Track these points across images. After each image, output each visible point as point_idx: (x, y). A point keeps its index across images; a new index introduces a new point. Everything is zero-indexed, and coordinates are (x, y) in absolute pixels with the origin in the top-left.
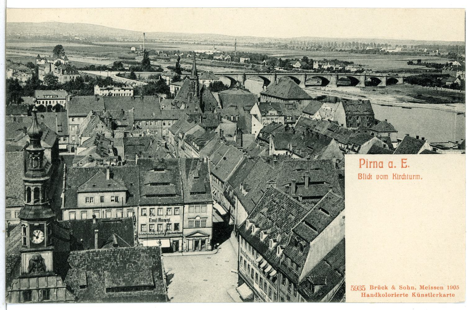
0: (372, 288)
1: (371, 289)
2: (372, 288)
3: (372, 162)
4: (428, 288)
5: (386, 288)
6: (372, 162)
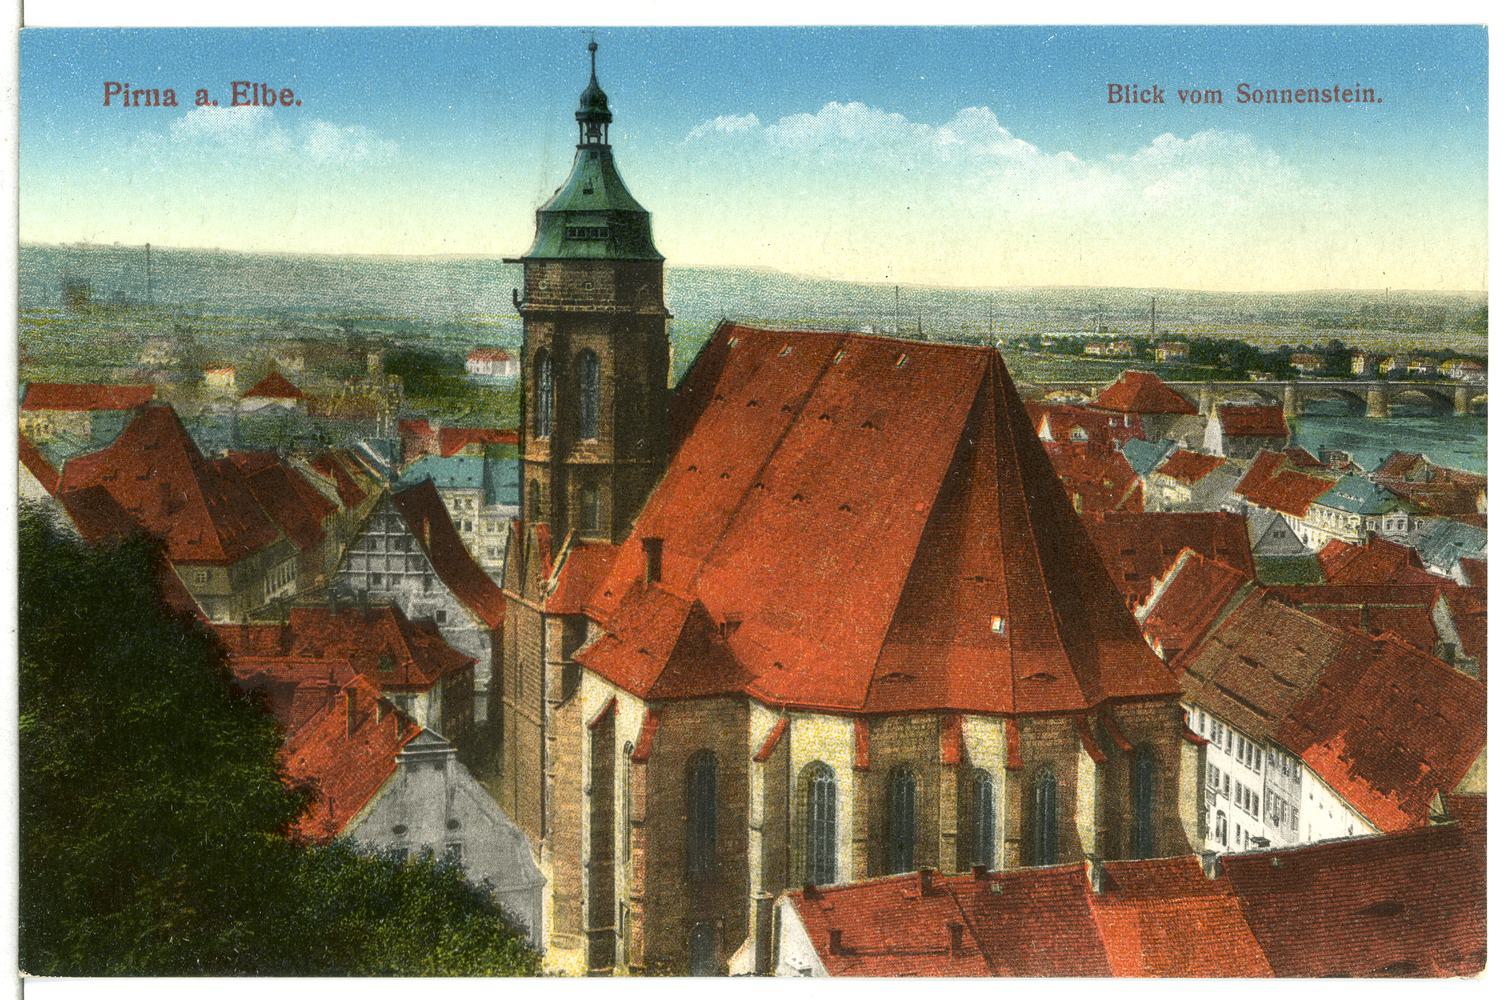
0: (1116, 97)
1: (1111, 101)
2: (1116, 97)
3: (142, 92)
5: (1159, 98)
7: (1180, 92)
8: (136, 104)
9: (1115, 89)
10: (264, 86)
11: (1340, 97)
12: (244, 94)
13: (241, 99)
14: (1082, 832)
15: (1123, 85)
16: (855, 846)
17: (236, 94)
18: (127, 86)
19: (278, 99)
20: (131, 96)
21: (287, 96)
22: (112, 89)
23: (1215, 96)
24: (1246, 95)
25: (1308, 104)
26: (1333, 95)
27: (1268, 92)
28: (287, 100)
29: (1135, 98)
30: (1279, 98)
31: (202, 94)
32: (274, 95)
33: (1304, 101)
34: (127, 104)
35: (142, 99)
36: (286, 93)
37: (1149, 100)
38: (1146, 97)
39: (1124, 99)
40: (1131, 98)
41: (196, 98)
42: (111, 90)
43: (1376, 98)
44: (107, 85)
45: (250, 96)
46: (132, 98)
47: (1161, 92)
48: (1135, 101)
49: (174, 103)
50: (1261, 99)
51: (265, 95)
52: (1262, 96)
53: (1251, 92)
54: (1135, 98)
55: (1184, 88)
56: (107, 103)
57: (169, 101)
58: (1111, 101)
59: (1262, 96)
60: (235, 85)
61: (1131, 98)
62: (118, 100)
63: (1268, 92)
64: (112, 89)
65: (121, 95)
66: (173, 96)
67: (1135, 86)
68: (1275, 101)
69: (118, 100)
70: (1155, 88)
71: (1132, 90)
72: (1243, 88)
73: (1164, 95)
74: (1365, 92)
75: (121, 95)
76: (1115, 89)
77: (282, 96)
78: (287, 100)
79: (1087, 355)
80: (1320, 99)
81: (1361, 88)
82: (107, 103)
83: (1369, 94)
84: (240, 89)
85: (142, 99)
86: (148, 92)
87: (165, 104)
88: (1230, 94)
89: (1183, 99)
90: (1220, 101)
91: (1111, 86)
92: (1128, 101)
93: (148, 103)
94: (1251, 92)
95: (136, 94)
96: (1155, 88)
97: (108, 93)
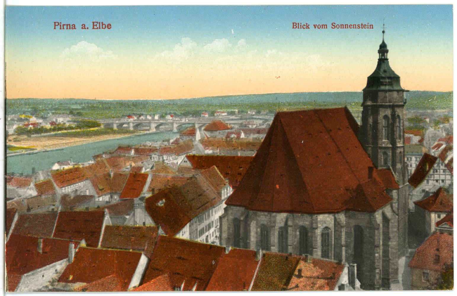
0: (295, 27)
1: (293, 28)
2: (295, 27)
3: (65, 25)
4: (367, 27)
5: (308, 27)
6: (65, 25)
7: (314, 25)
8: (63, 28)
9: (295, 24)
10: (102, 23)
11: (349, 27)
12: (96, 25)
13: (95, 27)
14: (195, 288)
15: (297, 23)
16: (317, 247)
17: (94, 25)
18: (61, 23)
19: (106, 26)
20: (62, 26)
21: (109, 26)
22: (57, 24)
23: (325, 26)
24: (334, 26)
25: (367, 29)
26: (361, 26)
27: (341, 25)
28: (109, 27)
29: (301, 27)
30: (344, 27)
31: (73, 26)
32: (337, 27)
33: (366, 28)
34: (61, 29)
35: (65, 27)
36: (109, 25)
37: (366, 28)
38: (304, 27)
39: (298, 27)
40: (300, 27)
41: (82, 27)
42: (56, 24)
43: (86, 27)
44: (55, 23)
45: (98, 26)
46: (62, 27)
47: (309, 25)
48: (301, 28)
49: (75, 28)
50: (339, 27)
51: (102, 25)
52: (320, 26)
53: (336, 25)
54: (301, 27)
55: (315, 24)
56: (55, 28)
57: (73, 28)
58: (293, 28)
59: (320, 26)
60: (93, 23)
61: (300, 27)
62: (58, 27)
63: (345, 25)
64: (57, 24)
65: (59, 26)
66: (75, 26)
67: (301, 23)
68: (343, 28)
69: (58, 27)
70: (307, 24)
71: (300, 24)
72: (333, 24)
73: (309, 26)
74: (370, 25)
75: (59, 26)
76: (295, 24)
77: (108, 26)
78: (109, 27)
79: (261, 119)
80: (357, 27)
81: (62, 24)
82: (55, 28)
83: (325, 26)
84: (95, 24)
85: (65, 27)
86: (67, 25)
87: (72, 28)
88: (329, 26)
89: (315, 27)
90: (327, 28)
91: (55, 23)
92: (298, 28)
93: (67, 28)
94: (336, 25)
95: (64, 25)
96: (307, 24)
97: (55, 25)
